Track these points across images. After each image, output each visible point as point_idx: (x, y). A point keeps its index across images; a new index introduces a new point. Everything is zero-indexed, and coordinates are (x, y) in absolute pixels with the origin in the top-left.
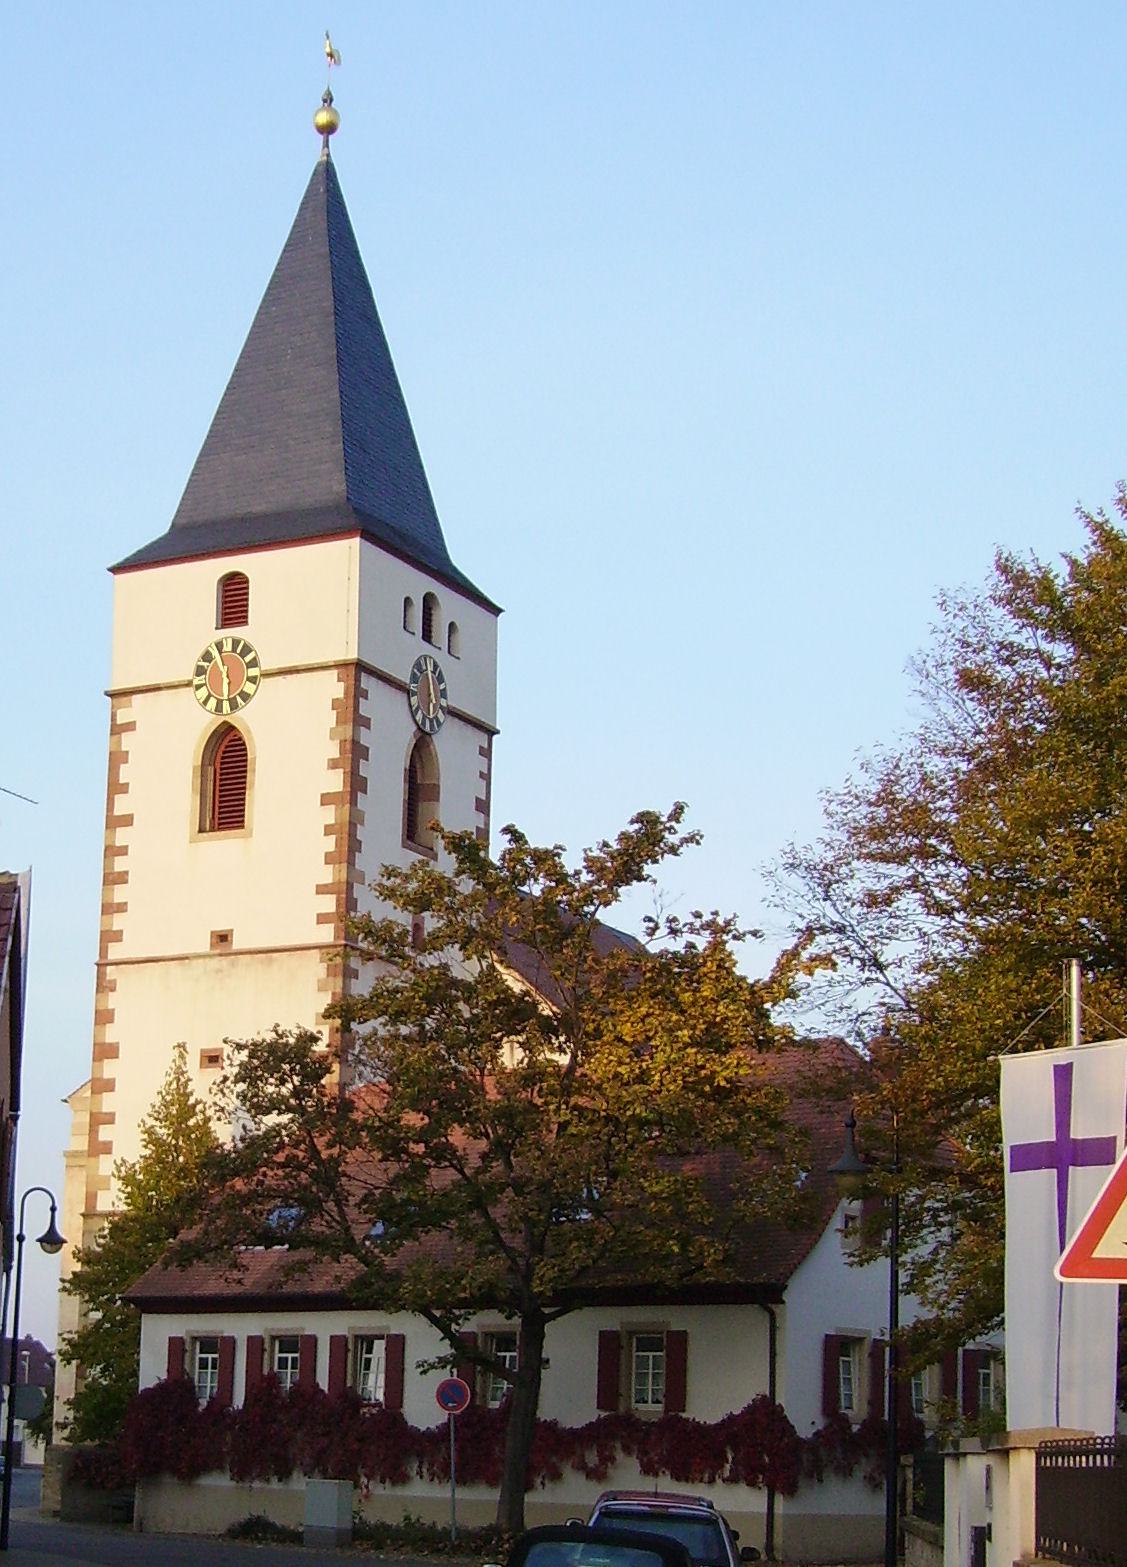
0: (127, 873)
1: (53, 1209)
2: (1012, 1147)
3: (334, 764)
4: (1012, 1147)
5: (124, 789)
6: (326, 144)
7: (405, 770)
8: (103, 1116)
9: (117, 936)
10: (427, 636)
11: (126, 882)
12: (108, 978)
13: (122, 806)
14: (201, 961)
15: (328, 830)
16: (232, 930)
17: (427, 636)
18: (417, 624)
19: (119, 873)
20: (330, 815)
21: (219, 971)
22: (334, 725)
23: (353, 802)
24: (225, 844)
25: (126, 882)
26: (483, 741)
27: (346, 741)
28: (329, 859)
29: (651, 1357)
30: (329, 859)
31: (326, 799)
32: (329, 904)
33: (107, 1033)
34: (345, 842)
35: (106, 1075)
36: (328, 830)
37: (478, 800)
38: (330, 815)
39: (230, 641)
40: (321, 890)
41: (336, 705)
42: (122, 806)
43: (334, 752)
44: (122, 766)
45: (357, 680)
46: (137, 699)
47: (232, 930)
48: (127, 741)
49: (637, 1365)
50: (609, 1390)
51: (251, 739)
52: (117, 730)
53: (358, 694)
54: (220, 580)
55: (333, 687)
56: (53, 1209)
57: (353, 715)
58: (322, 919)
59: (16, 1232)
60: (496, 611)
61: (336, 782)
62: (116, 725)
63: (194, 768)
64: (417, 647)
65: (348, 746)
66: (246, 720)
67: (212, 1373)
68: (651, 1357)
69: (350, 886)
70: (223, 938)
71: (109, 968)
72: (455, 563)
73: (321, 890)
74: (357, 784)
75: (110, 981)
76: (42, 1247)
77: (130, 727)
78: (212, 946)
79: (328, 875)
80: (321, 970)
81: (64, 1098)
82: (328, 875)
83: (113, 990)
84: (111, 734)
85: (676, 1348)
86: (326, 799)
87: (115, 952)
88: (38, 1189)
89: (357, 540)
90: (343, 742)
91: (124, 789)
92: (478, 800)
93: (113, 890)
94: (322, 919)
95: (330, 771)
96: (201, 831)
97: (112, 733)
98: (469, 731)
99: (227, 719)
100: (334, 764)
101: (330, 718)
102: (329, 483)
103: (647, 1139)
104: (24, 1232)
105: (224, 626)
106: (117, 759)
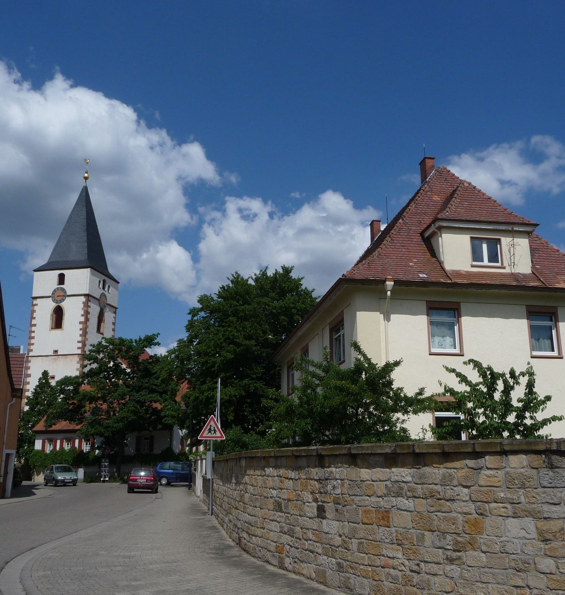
2: (6, 454)
3: (82, 315)
4: (6, 454)
5: (34, 318)
6: (86, 182)
7: (104, 323)
9: (32, 350)
10: (104, 288)
15: (81, 329)
17: (104, 288)
18: (101, 286)
20: (81, 326)
21: (55, 359)
23: (86, 323)
24: (58, 332)
26: (114, 310)
28: (81, 335)
30: (81, 335)
31: (80, 323)
32: (80, 345)
34: (84, 332)
36: (81, 329)
37: (113, 323)
38: (81, 326)
40: (79, 342)
41: (83, 303)
43: (82, 313)
46: (38, 300)
50: (138, 448)
53: (88, 301)
55: (83, 299)
57: (86, 305)
58: (79, 348)
60: (118, 283)
61: (83, 319)
66: (64, 305)
69: (85, 341)
70: (56, 351)
72: (110, 272)
73: (79, 342)
74: (87, 320)
77: (36, 305)
78: (53, 353)
79: (80, 339)
80: (78, 359)
82: (80, 339)
85: (152, 439)
86: (80, 323)
87: (31, 354)
91: (34, 318)
92: (113, 323)
94: (79, 348)
96: (52, 329)
98: (112, 308)
100: (82, 315)
101: (82, 306)
103: (326, 435)
105: (59, 285)
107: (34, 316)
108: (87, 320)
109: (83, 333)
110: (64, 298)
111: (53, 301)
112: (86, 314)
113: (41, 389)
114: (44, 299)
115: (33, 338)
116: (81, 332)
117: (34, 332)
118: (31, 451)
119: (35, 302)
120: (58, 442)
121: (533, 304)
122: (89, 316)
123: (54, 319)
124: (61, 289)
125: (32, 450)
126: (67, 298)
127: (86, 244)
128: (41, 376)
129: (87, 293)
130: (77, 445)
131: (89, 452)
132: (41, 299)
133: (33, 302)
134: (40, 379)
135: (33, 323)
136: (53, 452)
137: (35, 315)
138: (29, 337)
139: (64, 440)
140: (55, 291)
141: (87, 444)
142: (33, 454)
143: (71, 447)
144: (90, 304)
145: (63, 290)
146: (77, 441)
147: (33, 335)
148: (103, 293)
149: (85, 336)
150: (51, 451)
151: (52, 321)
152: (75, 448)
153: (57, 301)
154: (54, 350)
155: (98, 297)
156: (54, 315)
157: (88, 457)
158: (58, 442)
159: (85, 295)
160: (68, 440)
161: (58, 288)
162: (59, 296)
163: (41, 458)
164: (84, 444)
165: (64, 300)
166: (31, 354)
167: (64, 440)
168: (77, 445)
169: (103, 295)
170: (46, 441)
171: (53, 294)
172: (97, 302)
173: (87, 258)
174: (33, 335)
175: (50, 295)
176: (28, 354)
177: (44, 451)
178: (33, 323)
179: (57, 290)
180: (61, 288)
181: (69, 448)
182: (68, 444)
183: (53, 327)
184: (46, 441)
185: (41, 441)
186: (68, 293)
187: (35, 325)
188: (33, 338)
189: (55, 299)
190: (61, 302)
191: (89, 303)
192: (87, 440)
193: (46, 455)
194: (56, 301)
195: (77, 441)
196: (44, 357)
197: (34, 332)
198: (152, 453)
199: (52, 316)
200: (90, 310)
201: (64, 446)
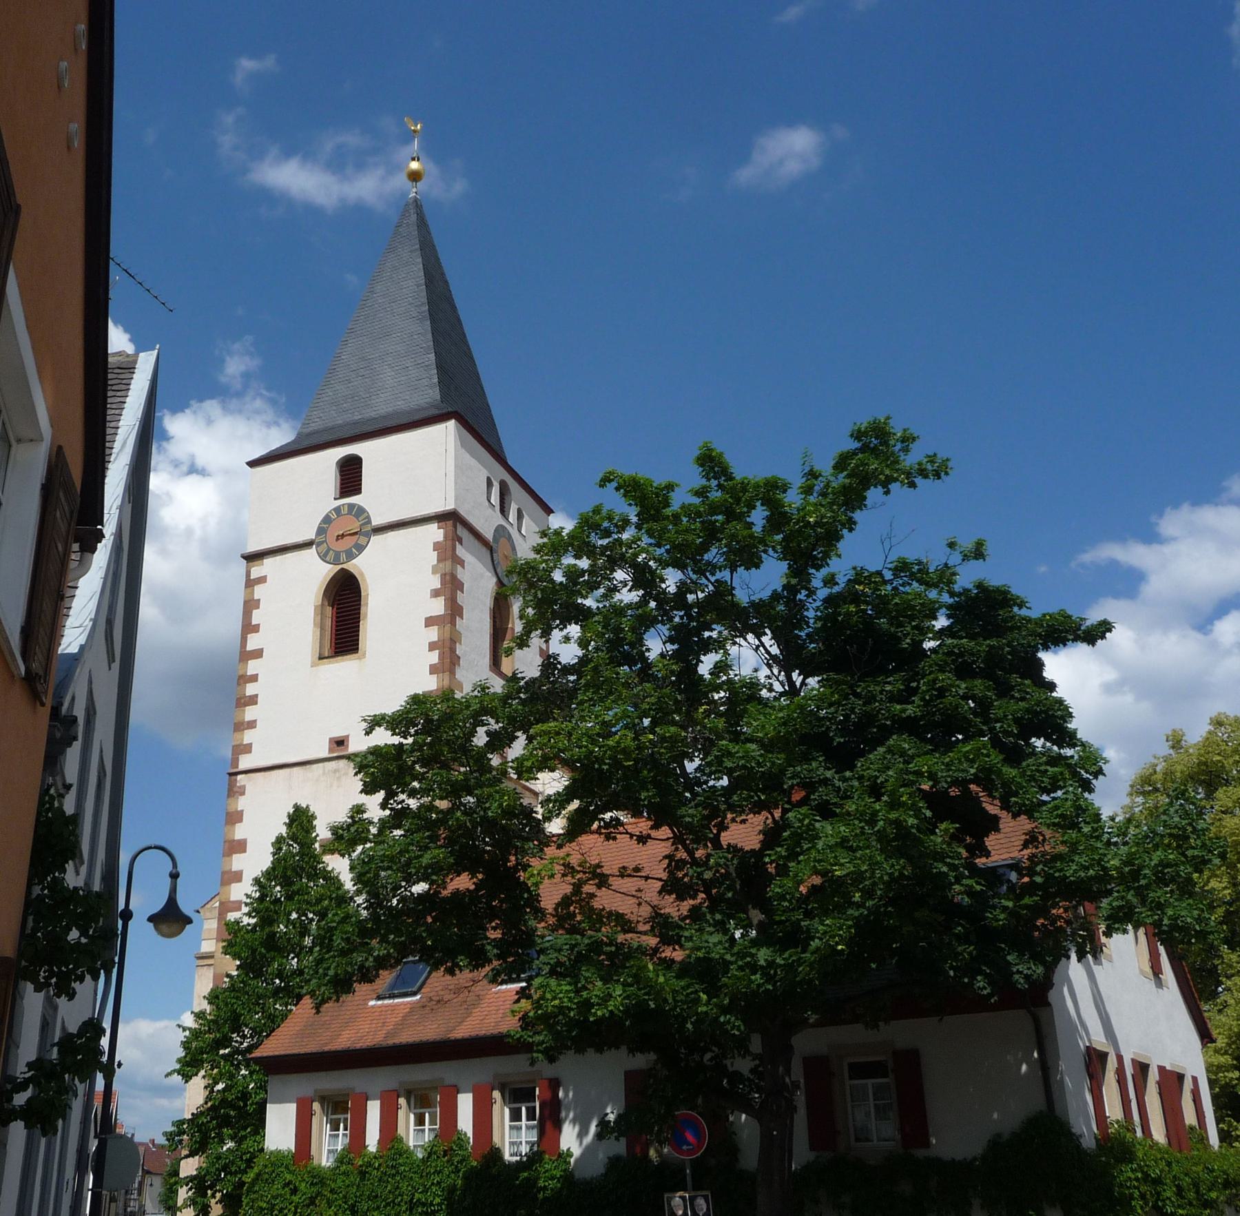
0: (256, 696)
1: (174, 876)
3: (436, 593)
5: (256, 629)
8: (230, 904)
9: (248, 749)
10: (504, 511)
11: (256, 703)
12: (238, 785)
13: (253, 643)
14: (321, 765)
15: (432, 646)
16: (348, 736)
17: (504, 511)
18: (495, 499)
19: (250, 696)
20: (433, 634)
21: (335, 771)
22: (435, 562)
23: (453, 623)
24: (345, 666)
25: (256, 703)
27: (445, 574)
28: (433, 670)
29: (870, 1087)
30: (433, 670)
31: (429, 622)
33: (236, 832)
34: (447, 654)
35: (235, 868)
38: (433, 634)
39: (346, 507)
41: (436, 546)
42: (253, 643)
43: (437, 584)
44: (254, 611)
45: (455, 527)
46: (268, 561)
47: (348, 736)
48: (259, 591)
49: (874, 1094)
51: (365, 580)
52: (250, 583)
54: (337, 463)
55: (435, 533)
56: (174, 876)
57: (447, 553)
59: (121, 906)
61: (438, 607)
62: (250, 579)
63: (316, 607)
64: (498, 520)
65: (448, 577)
67: (343, 1134)
68: (870, 1087)
71: (239, 777)
74: (455, 610)
75: (240, 787)
76: (156, 928)
77: (262, 580)
78: (331, 750)
81: (196, 909)
83: (243, 793)
84: (246, 587)
87: (245, 762)
88: (150, 848)
89: (453, 421)
90: (443, 576)
91: (256, 629)
93: (244, 710)
95: (433, 599)
96: (321, 658)
97: (247, 586)
99: (344, 566)
100: (436, 593)
101: (433, 557)
102: (428, 393)
104: (131, 907)
106: (251, 605)
107: (254, 622)
108: (455, 610)
109: (441, 657)
110: (362, 540)
111: (323, 557)
112: (451, 587)
113: (286, 882)
114: (290, 556)
115: (253, 700)
116: (434, 657)
117: (254, 678)
118: (250, 1163)
119: (256, 572)
120: (374, 1110)
121: (17, 1183)
122: (461, 598)
123: (328, 623)
124: (350, 512)
125: (253, 1156)
126: (375, 539)
127: (432, 356)
128: (284, 831)
129: (450, 506)
130: (465, 1121)
131: (534, 1158)
132: (279, 559)
133: (248, 574)
134: (279, 841)
135: (250, 646)
136: (350, 1162)
137: (257, 617)
138: (238, 700)
139: (402, 1101)
140: (327, 520)
141: (516, 1116)
142: (259, 1175)
143: (440, 1135)
144: (461, 551)
145: (360, 511)
146: (465, 1104)
147: (250, 689)
148: (501, 526)
149: (452, 672)
150: (342, 1159)
151: (322, 629)
152: (461, 1138)
153: (337, 554)
154: (331, 740)
155: (489, 535)
156: (329, 610)
157: (531, 1183)
158: (374, 1110)
159: (440, 518)
160: (421, 1100)
161: (337, 510)
162: (343, 536)
163: (295, 1191)
164: (501, 1113)
165: (361, 549)
166: (245, 762)
167: (402, 1101)
168: (465, 1121)
169: (500, 531)
170: (316, 1106)
171: (321, 531)
172: (485, 553)
173: (438, 397)
174: (250, 689)
175: (310, 535)
176: (235, 762)
177: (309, 1157)
178: (250, 646)
179: (334, 516)
180: (351, 506)
181: (427, 1137)
182: (420, 1121)
183: (338, 496)
184: (316, 1106)
185: (292, 1108)
186: (377, 521)
187: (258, 654)
188: (253, 700)
189: (329, 549)
190: (351, 556)
191: (458, 546)
192: (518, 1095)
193: (319, 1178)
194: (331, 555)
195: (465, 1104)
196: (295, 769)
197: (254, 678)
198: (920, 1153)
199: (320, 611)
200: (461, 574)
201: (401, 1131)
